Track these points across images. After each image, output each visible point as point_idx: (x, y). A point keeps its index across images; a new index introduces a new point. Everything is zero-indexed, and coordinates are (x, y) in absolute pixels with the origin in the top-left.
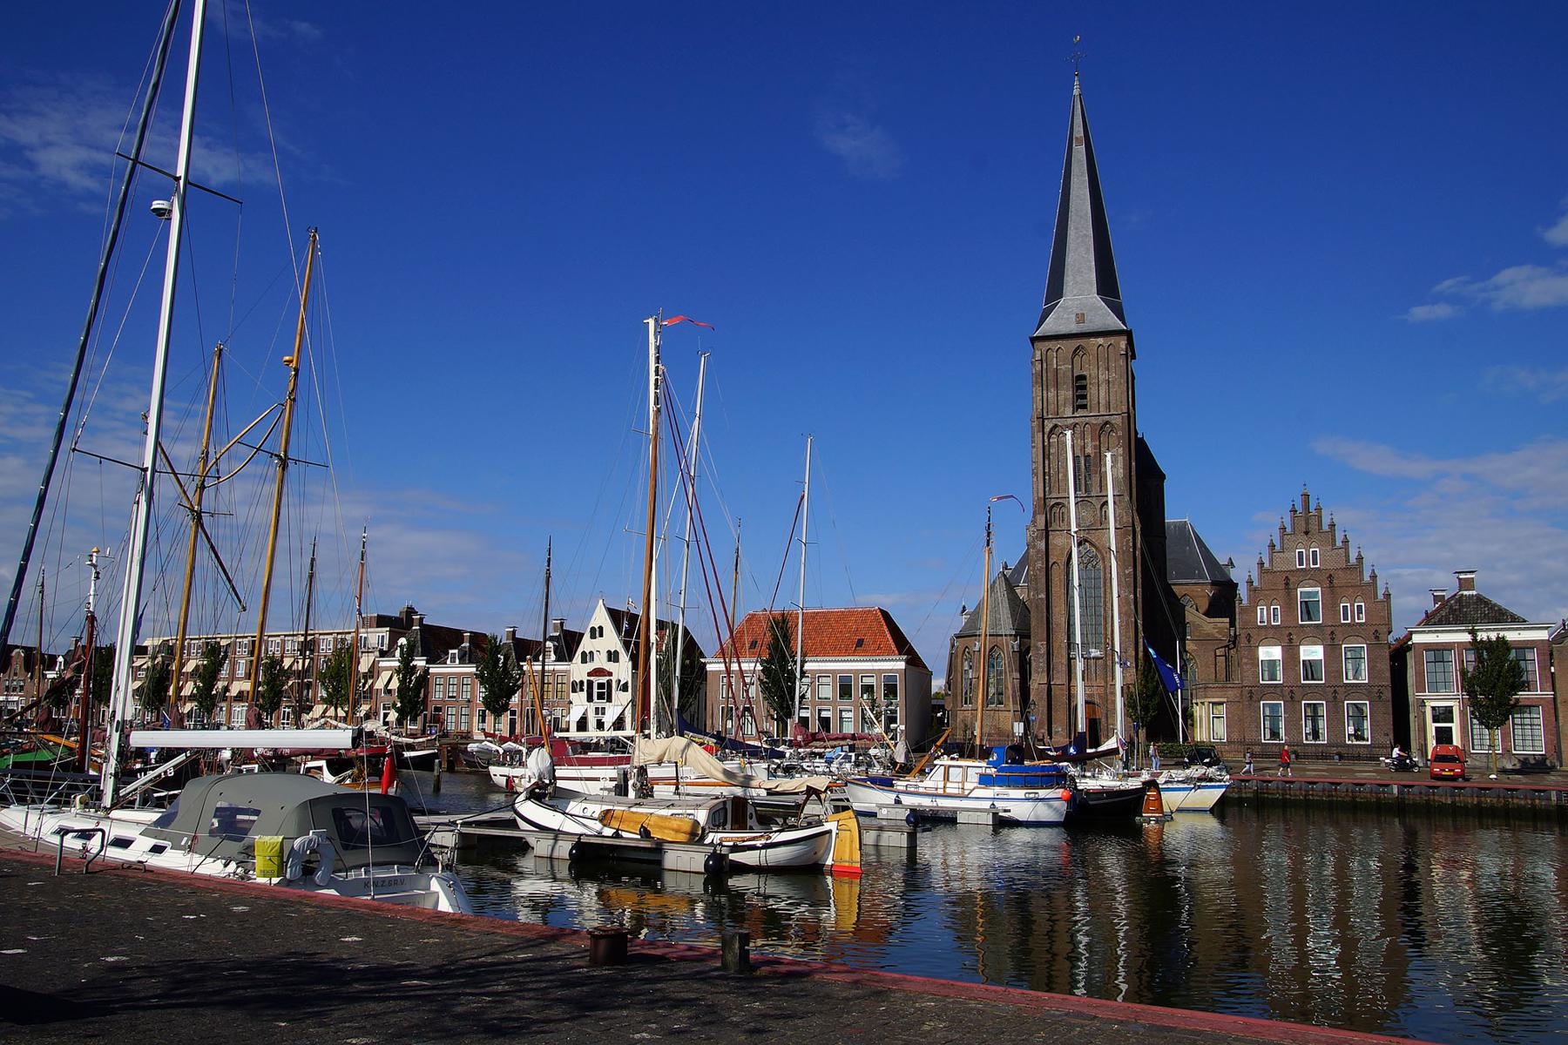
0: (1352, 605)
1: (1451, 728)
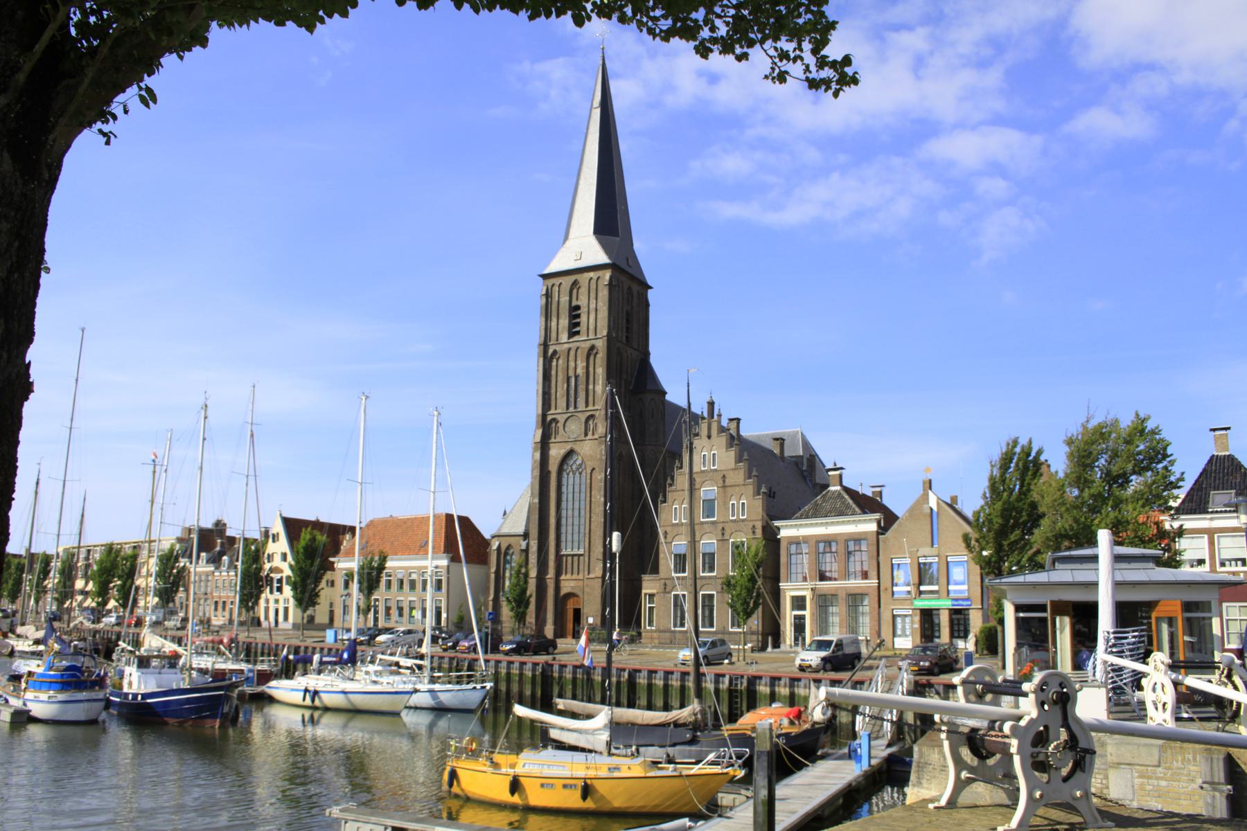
0: (738, 503)
1: (804, 616)
